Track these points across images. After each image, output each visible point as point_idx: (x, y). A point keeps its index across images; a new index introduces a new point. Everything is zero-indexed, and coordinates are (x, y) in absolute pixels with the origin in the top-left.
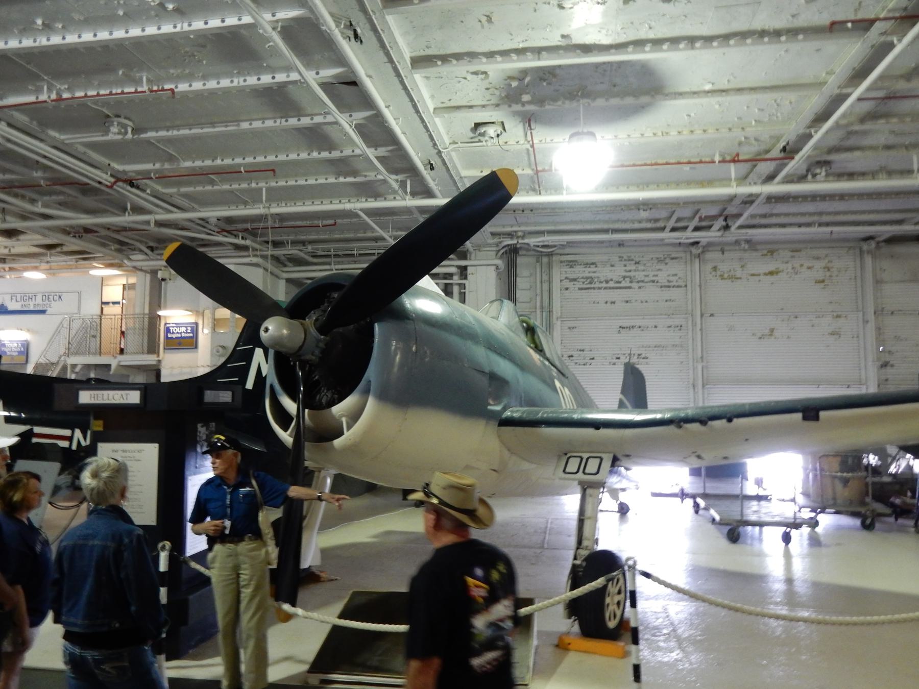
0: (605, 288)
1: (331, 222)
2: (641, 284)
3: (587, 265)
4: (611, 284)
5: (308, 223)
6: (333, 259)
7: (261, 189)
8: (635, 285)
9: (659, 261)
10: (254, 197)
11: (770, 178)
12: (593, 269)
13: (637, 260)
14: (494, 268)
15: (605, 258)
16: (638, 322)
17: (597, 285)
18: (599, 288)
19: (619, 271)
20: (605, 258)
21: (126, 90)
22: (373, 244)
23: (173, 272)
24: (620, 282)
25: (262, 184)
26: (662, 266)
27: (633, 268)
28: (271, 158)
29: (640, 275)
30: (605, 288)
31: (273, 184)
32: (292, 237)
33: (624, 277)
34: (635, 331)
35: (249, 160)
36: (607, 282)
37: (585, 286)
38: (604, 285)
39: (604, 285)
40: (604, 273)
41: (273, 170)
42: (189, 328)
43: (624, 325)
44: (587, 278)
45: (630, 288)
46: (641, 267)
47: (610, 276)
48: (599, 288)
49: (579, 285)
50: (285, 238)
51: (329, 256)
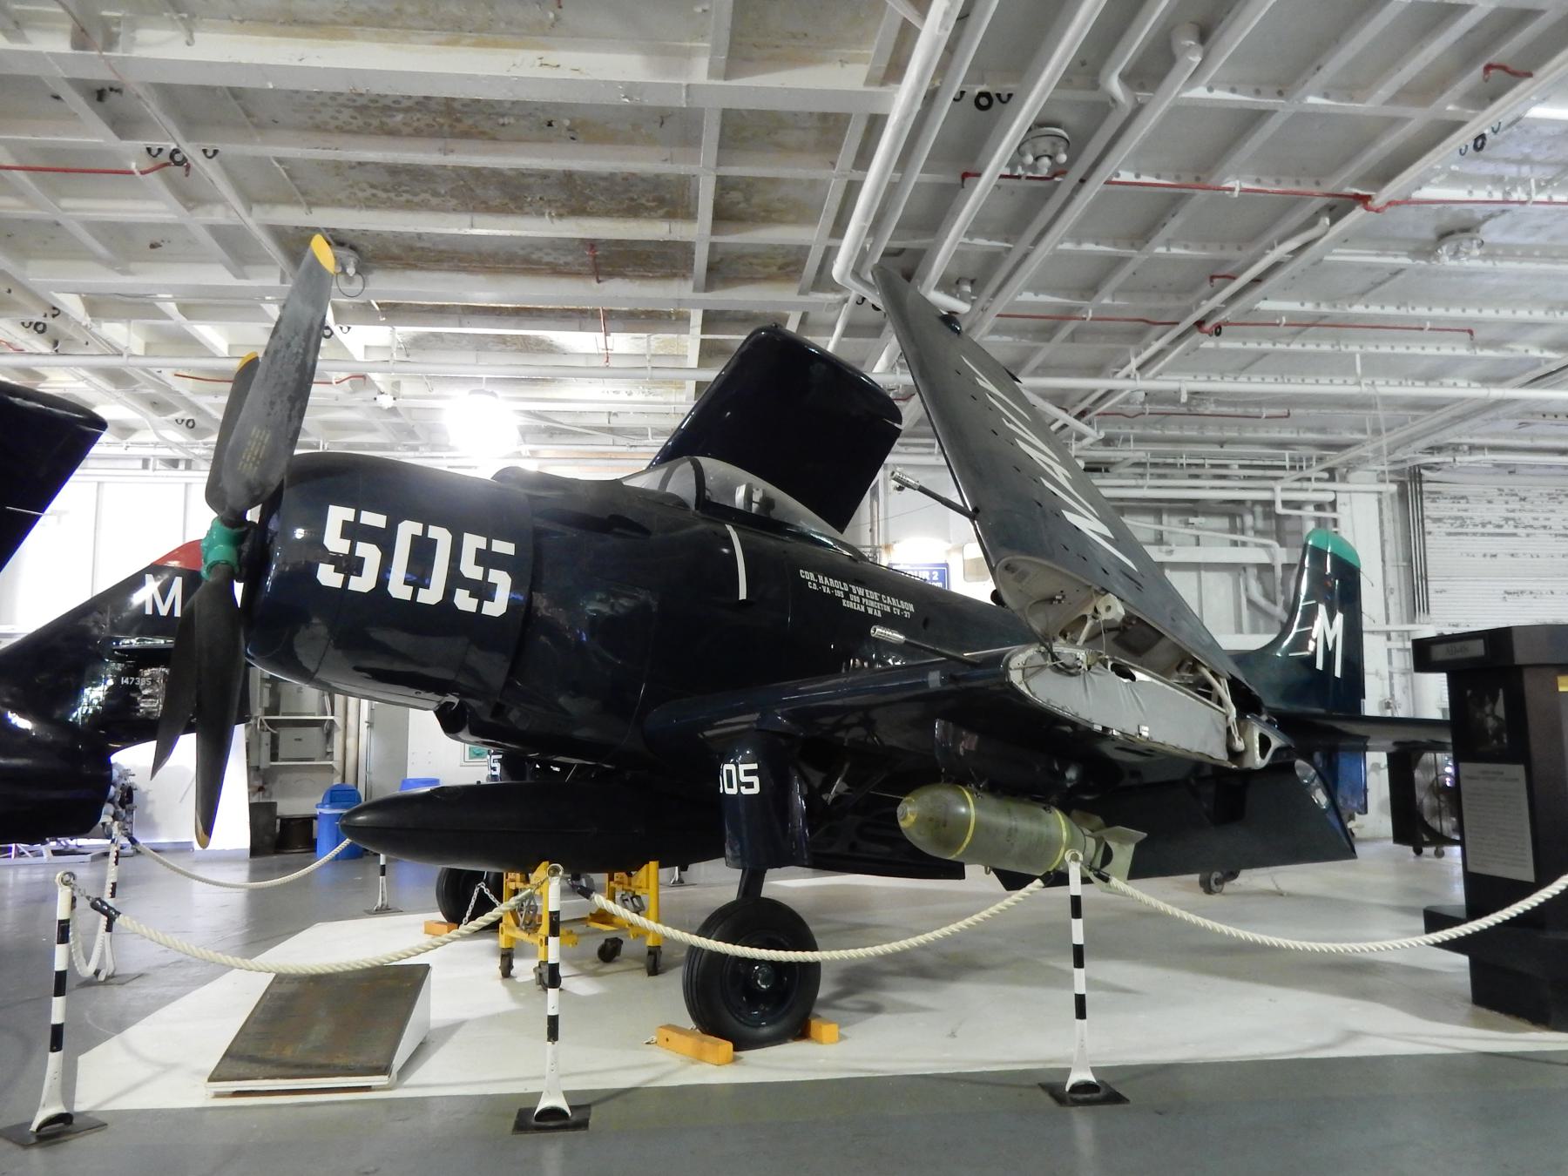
0: (1483, 534)
1: (1283, 411)
2: (1530, 531)
3: (1457, 498)
4: (1489, 529)
5: (1240, 411)
6: (1150, 470)
7: (1353, 355)
8: (1520, 531)
9: (1551, 497)
10: (1344, 366)
11: (1109, 393)
12: (1463, 504)
13: (1523, 494)
14: (1375, 496)
15: (1480, 489)
16: (1527, 586)
17: (1471, 529)
18: (1475, 534)
19: (1497, 512)
20: (1480, 489)
21: (1556, 198)
22: (1217, 449)
23: (881, 474)
24: (1500, 526)
25: (1354, 348)
26: (1554, 506)
27: (1517, 506)
28: (1472, 313)
29: (1526, 518)
30: (1483, 534)
31: (1372, 349)
32: (1138, 431)
33: (1507, 519)
34: (1526, 598)
35: (1439, 312)
36: (1484, 525)
37: (1453, 530)
38: (1480, 529)
39: (1480, 529)
40: (1479, 511)
41: (1471, 332)
42: (936, 574)
43: (1512, 589)
44: (1456, 518)
45: (1514, 535)
46: (1528, 506)
47: (1488, 516)
48: (1475, 534)
49: (1446, 528)
50: (1126, 430)
51: (1283, 468)
